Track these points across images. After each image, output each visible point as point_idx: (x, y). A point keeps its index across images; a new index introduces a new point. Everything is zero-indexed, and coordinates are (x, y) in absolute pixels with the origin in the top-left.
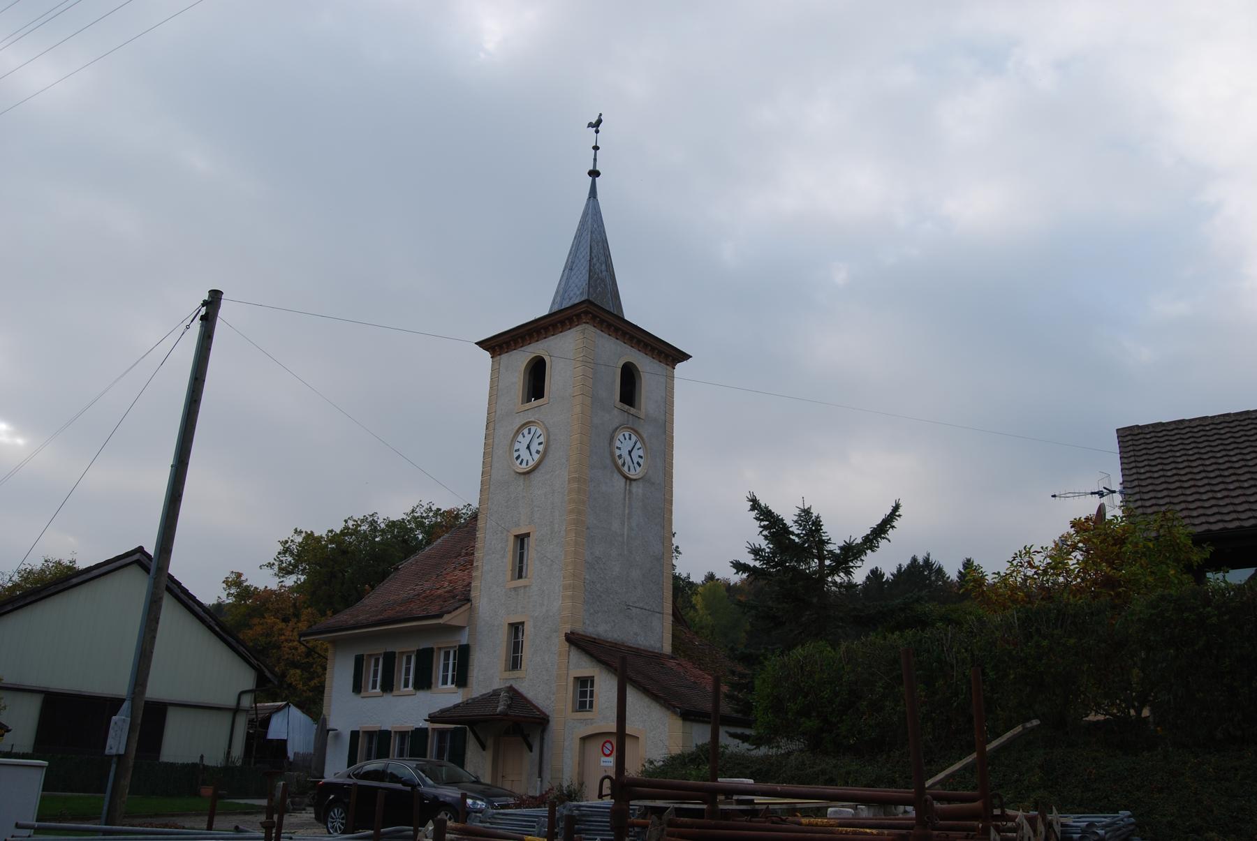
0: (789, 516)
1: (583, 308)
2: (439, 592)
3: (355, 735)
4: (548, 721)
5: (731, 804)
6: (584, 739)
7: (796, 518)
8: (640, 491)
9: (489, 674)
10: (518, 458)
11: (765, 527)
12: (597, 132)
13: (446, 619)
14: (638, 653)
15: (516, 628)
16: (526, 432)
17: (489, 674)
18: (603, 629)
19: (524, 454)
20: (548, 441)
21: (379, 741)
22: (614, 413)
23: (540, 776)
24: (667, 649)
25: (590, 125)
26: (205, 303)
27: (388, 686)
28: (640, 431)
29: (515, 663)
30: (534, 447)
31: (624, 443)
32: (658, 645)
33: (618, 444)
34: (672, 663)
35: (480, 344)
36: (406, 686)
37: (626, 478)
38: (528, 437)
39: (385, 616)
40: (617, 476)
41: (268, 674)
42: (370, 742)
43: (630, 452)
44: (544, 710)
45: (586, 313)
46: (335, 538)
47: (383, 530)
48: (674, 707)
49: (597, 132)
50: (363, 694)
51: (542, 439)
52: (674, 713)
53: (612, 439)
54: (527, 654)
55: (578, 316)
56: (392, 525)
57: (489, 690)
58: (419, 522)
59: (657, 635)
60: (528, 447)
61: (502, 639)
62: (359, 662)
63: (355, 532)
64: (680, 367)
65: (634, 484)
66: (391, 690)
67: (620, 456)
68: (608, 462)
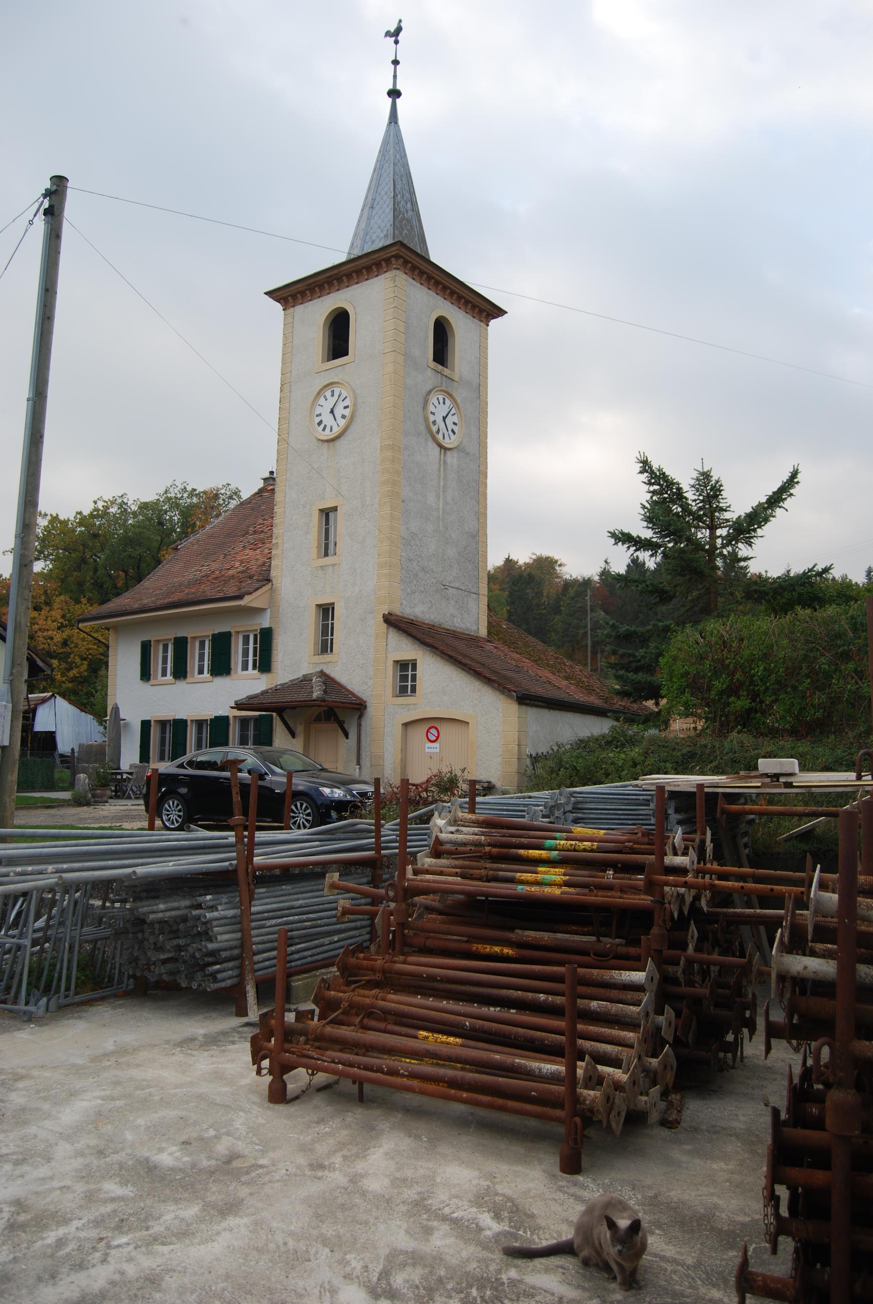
0: (685, 478)
1: (393, 251)
2: (231, 572)
3: (146, 725)
4: (365, 707)
5: (779, 787)
6: (406, 725)
7: (692, 482)
8: (455, 461)
9: (294, 659)
10: (320, 423)
11: (654, 493)
12: (396, 42)
13: (246, 601)
14: (455, 635)
15: (326, 611)
16: (328, 394)
17: (294, 659)
18: (419, 610)
19: (328, 419)
20: (355, 405)
21: (176, 731)
22: (427, 372)
23: (358, 763)
24: (483, 632)
25: (388, 34)
26: (48, 194)
27: (180, 672)
28: (454, 394)
29: (325, 646)
30: (339, 412)
31: (439, 408)
32: (474, 628)
33: (431, 408)
34: (489, 647)
35: (266, 293)
36: (164, 674)
37: (441, 446)
38: (332, 401)
39: (175, 598)
40: (432, 445)
41: (40, 663)
42: (163, 732)
43: (444, 418)
44: (360, 695)
45: (397, 257)
46: (83, 521)
47: (134, 513)
48: (510, 690)
49: (396, 42)
50: (152, 682)
51: (347, 402)
52: (510, 697)
53: (426, 402)
54: (338, 636)
55: (388, 261)
56: (144, 506)
57: (299, 675)
58: (174, 503)
59: (472, 617)
60: (332, 412)
61: (310, 621)
62: (146, 648)
63: (105, 513)
64: (495, 324)
65: (448, 453)
66: (185, 677)
67: (434, 422)
68: (422, 428)
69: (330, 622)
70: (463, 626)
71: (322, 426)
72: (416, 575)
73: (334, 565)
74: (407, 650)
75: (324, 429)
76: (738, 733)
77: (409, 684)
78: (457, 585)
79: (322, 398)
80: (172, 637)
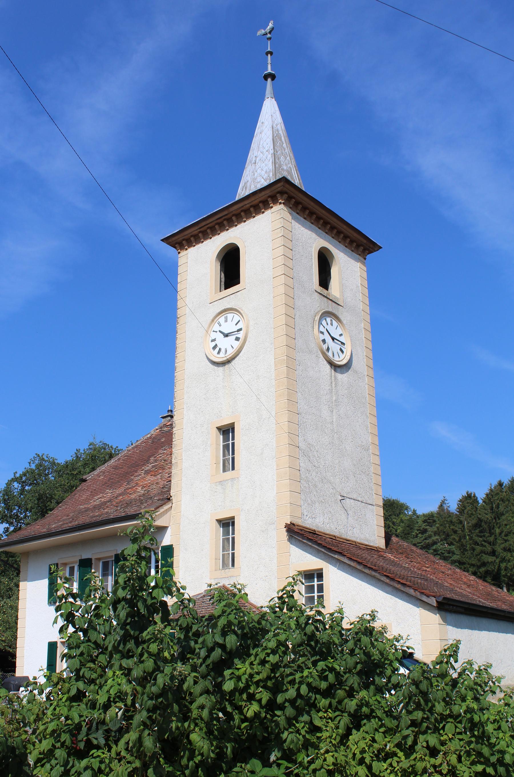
22: (311, 301)
28: (340, 317)
35: (162, 240)
45: (282, 193)
69: (231, 536)
70: (362, 536)
71: (217, 350)
72: (315, 486)
73: (233, 479)
74: (311, 561)
75: (219, 353)
76: (456, 661)
77: (316, 594)
78: (355, 497)
79: (216, 324)
80: (77, 559)
